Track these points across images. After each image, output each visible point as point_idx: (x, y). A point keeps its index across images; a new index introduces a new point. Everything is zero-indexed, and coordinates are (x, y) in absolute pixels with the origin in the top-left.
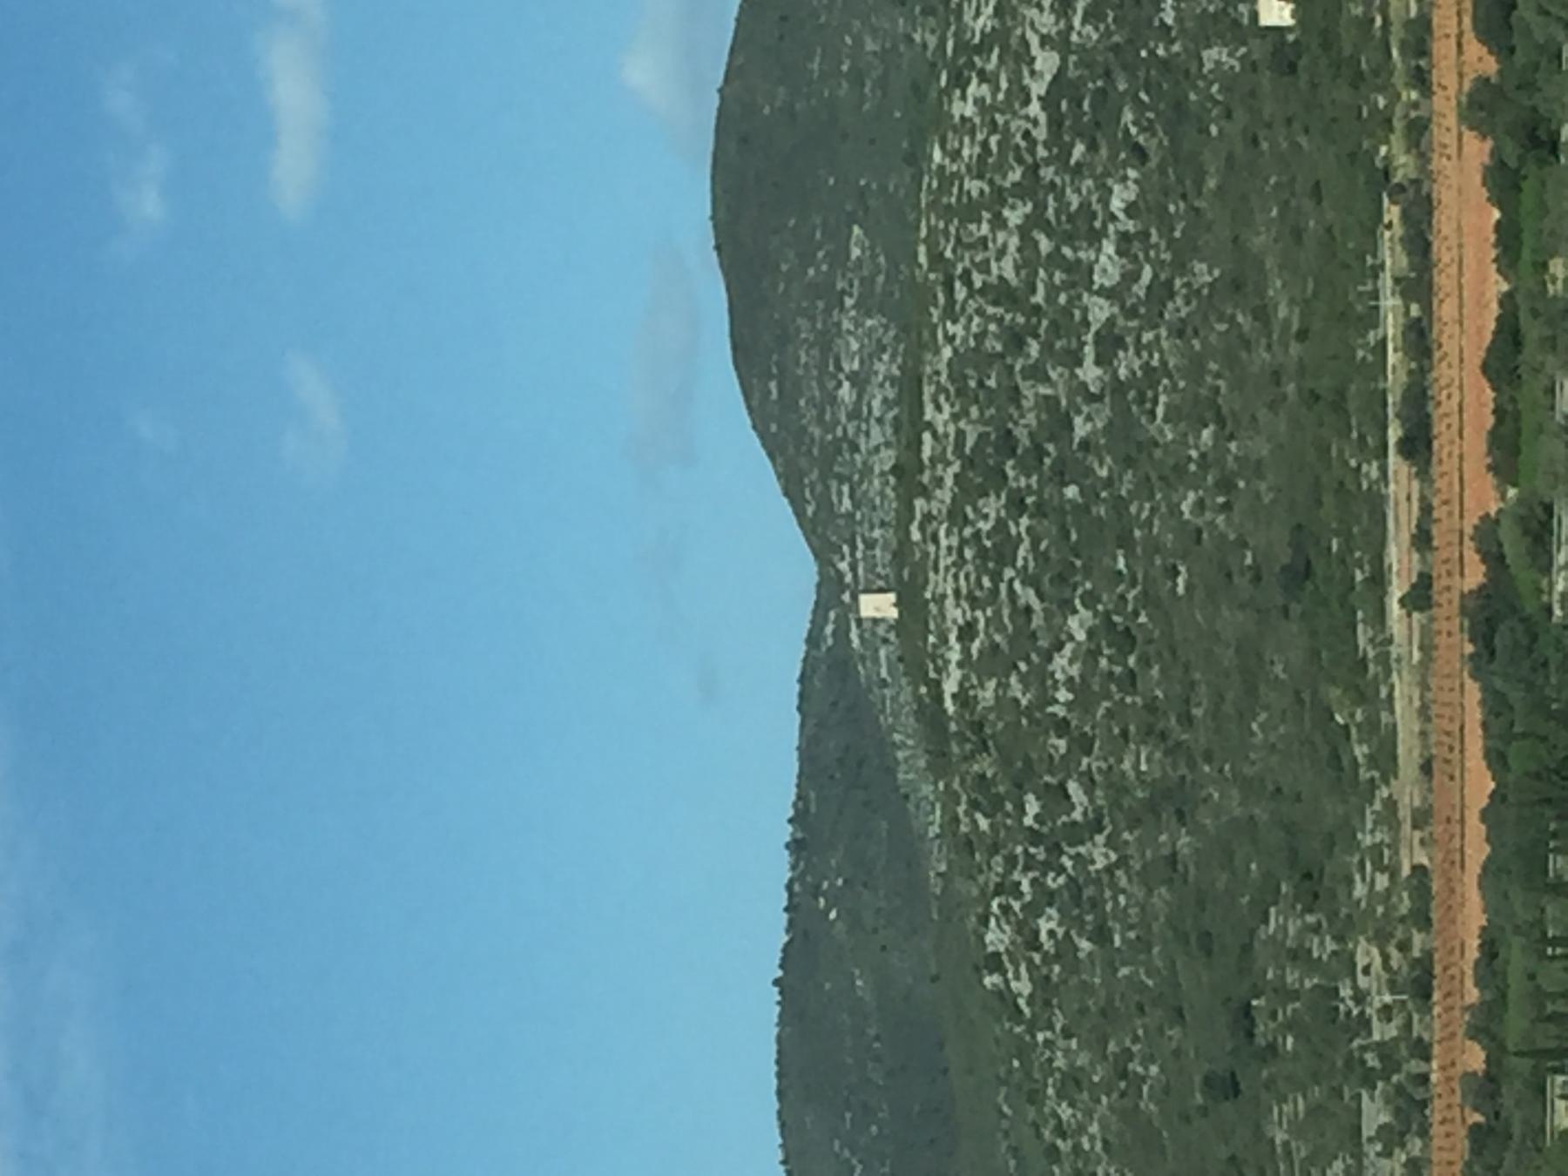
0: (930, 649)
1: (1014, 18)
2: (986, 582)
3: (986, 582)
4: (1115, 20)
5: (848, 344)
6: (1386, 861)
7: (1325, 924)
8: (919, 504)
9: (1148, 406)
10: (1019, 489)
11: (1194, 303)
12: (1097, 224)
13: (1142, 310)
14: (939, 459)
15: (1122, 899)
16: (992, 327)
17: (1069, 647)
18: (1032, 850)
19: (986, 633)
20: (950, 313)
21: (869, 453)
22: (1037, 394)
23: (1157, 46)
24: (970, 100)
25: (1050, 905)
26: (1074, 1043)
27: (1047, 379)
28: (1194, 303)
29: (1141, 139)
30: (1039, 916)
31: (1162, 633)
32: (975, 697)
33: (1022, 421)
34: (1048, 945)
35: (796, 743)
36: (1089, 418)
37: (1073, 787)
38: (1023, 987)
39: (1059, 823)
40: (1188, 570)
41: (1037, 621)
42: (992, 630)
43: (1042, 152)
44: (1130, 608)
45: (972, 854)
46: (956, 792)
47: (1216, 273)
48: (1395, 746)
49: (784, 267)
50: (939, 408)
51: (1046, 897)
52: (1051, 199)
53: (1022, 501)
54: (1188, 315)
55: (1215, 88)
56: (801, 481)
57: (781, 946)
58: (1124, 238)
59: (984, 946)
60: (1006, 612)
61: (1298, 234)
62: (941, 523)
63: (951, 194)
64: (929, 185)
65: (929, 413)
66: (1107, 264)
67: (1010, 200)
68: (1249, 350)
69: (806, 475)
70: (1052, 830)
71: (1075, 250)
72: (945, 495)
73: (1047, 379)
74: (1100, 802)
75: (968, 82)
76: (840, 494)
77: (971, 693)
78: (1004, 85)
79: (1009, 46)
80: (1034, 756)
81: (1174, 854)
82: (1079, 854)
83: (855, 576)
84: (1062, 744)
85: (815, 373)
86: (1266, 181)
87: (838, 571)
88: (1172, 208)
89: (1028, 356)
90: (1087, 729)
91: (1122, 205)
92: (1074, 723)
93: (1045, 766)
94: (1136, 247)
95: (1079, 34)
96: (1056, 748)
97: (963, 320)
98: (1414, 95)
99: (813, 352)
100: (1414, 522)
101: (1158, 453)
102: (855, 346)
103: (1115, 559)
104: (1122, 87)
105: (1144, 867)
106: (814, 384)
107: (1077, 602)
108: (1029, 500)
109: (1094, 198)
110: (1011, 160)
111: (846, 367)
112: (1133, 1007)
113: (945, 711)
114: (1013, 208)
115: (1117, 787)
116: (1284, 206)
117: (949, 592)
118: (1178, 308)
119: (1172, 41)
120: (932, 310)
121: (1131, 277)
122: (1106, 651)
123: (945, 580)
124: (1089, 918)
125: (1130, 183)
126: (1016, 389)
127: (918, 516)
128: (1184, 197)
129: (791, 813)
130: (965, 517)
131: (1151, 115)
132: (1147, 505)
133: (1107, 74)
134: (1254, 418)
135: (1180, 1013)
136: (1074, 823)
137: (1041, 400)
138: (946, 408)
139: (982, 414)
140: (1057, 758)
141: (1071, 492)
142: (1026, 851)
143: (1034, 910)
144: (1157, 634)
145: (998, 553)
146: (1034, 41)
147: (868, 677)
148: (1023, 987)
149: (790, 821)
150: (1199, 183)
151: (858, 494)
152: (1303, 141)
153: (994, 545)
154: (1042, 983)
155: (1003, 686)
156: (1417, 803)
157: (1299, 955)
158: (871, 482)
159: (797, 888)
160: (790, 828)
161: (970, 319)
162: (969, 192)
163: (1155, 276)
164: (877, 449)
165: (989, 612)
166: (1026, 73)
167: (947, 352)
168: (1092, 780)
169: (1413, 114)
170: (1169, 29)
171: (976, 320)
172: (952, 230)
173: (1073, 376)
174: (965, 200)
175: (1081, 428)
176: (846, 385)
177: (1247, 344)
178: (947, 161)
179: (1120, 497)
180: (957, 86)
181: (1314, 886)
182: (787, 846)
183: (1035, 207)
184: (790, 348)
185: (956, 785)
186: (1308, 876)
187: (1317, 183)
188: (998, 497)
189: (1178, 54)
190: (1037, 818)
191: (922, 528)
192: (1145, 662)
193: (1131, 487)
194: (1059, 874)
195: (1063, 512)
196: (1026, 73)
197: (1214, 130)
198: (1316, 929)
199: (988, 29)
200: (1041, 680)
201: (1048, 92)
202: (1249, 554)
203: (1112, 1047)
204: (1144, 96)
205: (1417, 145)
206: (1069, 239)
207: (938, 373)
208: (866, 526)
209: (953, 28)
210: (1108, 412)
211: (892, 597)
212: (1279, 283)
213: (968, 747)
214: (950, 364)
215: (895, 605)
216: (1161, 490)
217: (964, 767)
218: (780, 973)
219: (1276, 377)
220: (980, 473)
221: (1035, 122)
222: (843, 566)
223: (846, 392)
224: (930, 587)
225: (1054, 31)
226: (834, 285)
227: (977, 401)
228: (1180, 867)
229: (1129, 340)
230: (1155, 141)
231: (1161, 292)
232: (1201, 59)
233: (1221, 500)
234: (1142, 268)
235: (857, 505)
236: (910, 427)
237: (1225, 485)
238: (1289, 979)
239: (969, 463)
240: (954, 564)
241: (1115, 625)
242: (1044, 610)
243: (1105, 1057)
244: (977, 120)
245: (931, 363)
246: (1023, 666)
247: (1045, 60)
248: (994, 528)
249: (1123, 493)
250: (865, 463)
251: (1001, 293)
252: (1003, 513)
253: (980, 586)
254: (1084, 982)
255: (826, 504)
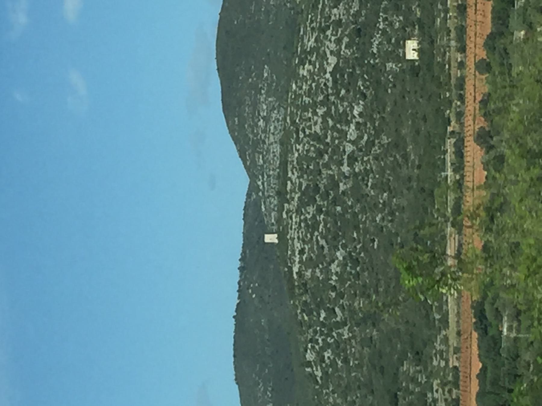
0: (289, 256)
1: (321, 44)
2: (309, 235)
3: (309, 235)
4: (356, 49)
5: (262, 106)
6: (444, 357)
7: (423, 371)
8: (286, 205)
9: (365, 182)
10: (320, 205)
11: (382, 149)
12: (349, 118)
13: (364, 150)
14: (293, 191)
15: (353, 349)
16: (312, 149)
17: (336, 262)
18: (323, 329)
19: (308, 252)
20: (298, 141)
21: (269, 145)
22: (327, 173)
23: (370, 60)
24: (306, 70)
25: (329, 348)
26: (336, 395)
27: (331, 169)
28: (382, 149)
29: (364, 91)
30: (325, 351)
31: (369, 261)
32: (304, 274)
33: (322, 182)
34: (327, 361)
35: (242, 231)
36: (345, 184)
37: (337, 310)
38: (319, 374)
39: (332, 321)
40: (378, 241)
41: (326, 251)
42: (310, 252)
43: (330, 91)
44: (358, 251)
45: (302, 327)
46: (297, 306)
47: (390, 140)
48: (448, 318)
49: (241, 78)
50: (293, 174)
51: (327, 346)
52: (333, 108)
53: (321, 209)
54: (380, 153)
55: (390, 77)
56: (246, 153)
57: (236, 304)
58: (358, 123)
59: (306, 359)
60: (315, 247)
61: (418, 132)
62: (293, 213)
63: (299, 101)
64: (291, 96)
65: (290, 174)
66: (352, 132)
67: (319, 106)
68: (401, 168)
69: (247, 151)
70: (330, 323)
71: (341, 126)
72: (295, 203)
73: (331, 169)
74: (346, 316)
75: (305, 64)
76: (259, 158)
77: (303, 272)
78: (318, 66)
79: (320, 53)
80: (324, 297)
81: (371, 337)
82: (339, 332)
83: (264, 187)
84: (333, 294)
85: (251, 116)
86: (408, 112)
87: (257, 184)
88: (375, 116)
89: (324, 160)
90: (342, 290)
91: (358, 113)
92: (338, 288)
93: (327, 302)
94: (362, 127)
95: (344, 52)
96: (332, 296)
97: (301, 145)
98: (459, 103)
99: (250, 108)
100: (456, 249)
101: (369, 199)
102: (265, 107)
103: (353, 234)
104: (358, 72)
105: (361, 340)
106: (251, 120)
107: (340, 247)
108: (324, 209)
109: (348, 109)
110: (320, 93)
111: (261, 114)
112: (356, 387)
113: (293, 277)
114: (320, 109)
115: (352, 312)
116: (413, 122)
117: (296, 237)
118: (376, 150)
119: (376, 59)
120: (291, 139)
121: (361, 137)
122: (350, 265)
123: (294, 232)
124: (342, 354)
125: (360, 105)
126: (320, 171)
127: (285, 210)
128: (379, 113)
129: (240, 257)
130: (302, 212)
131: (368, 83)
132: (364, 216)
133: (354, 68)
134: (402, 192)
135: (373, 392)
136: (338, 322)
137: (328, 176)
138: (296, 174)
139: (308, 177)
140: (332, 300)
141: (339, 208)
142: (320, 329)
143: (323, 349)
144: (367, 260)
145: (313, 226)
146: (328, 53)
147: (267, 222)
148: (319, 374)
149: (240, 260)
150: (384, 109)
151: (265, 158)
152: (421, 100)
153: (312, 223)
154: (325, 373)
155: (314, 272)
156: (455, 345)
157: (414, 380)
158: (269, 155)
159: (242, 284)
160: (239, 263)
161: (304, 145)
162: (305, 102)
163: (369, 138)
164: (272, 144)
165: (309, 246)
166: (325, 63)
167: (296, 155)
168: (344, 308)
169: (458, 110)
170: (375, 54)
171: (307, 145)
172: (299, 113)
173: (339, 169)
174: (303, 103)
175: (342, 187)
176: (262, 120)
177: (400, 166)
178: (298, 89)
179: (355, 212)
180: (301, 65)
181: (420, 358)
182: (239, 269)
183: (327, 109)
184: (242, 107)
185: (297, 303)
186: (418, 353)
187: (425, 116)
188: (313, 207)
189: (377, 63)
190: (324, 318)
191: (287, 213)
192: (363, 270)
193: (359, 209)
194: (332, 338)
195: (335, 215)
196: (325, 63)
197: (389, 91)
198: (420, 372)
199: (312, 46)
200: (327, 271)
201: (333, 71)
202: (399, 239)
203: (349, 398)
204: (365, 76)
205: (460, 120)
206: (340, 122)
207: (293, 161)
208: (268, 170)
209: (300, 44)
210: (351, 182)
211: (276, 235)
212: (411, 147)
213: (301, 291)
214: (297, 159)
215: (277, 238)
216: (369, 212)
217: (300, 298)
218: (235, 314)
219: (410, 179)
220: (308, 196)
221: (328, 80)
222: (260, 183)
223: (261, 123)
224: (289, 235)
225: (335, 49)
226: (258, 86)
227: (306, 173)
228: (374, 342)
229: (359, 159)
230: (369, 92)
231: (371, 143)
232: (386, 66)
233: (390, 218)
234: (364, 135)
235: (264, 162)
236: (283, 178)
237: (392, 213)
238: (411, 388)
239: (303, 194)
240: (297, 228)
241: (353, 256)
242: (328, 248)
243: (346, 402)
244: (308, 77)
245: (290, 157)
246: (321, 266)
247: (331, 59)
248: (311, 217)
249: (356, 211)
250: (268, 148)
251: (316, 137)
252: (315, 212)
253: (307, 237)
254: (340, 375)
255: (253, 162)
